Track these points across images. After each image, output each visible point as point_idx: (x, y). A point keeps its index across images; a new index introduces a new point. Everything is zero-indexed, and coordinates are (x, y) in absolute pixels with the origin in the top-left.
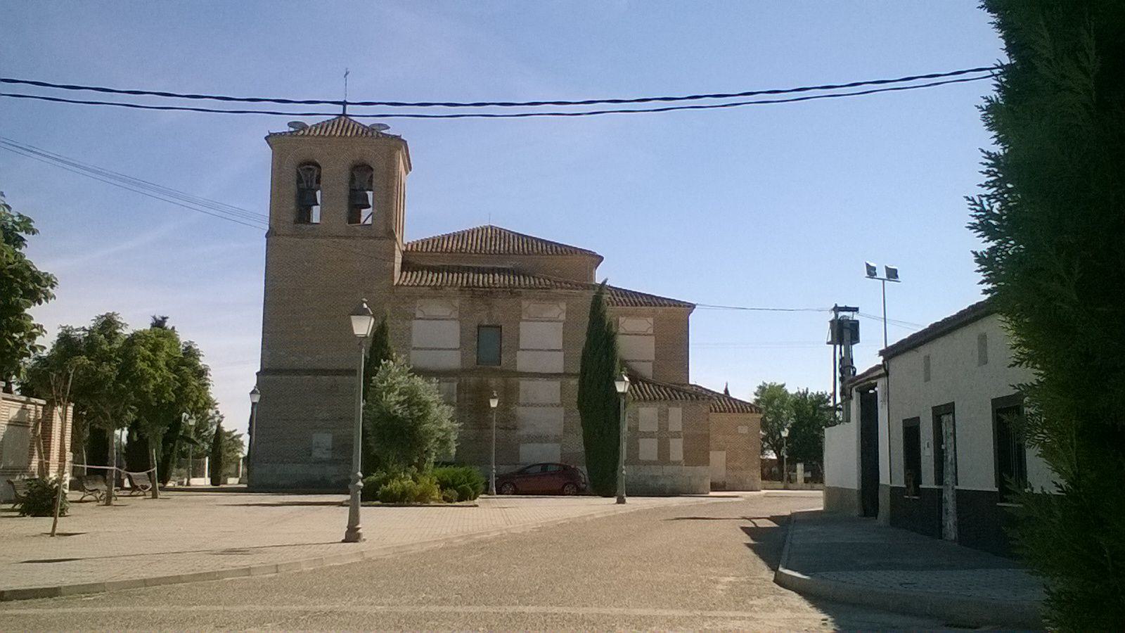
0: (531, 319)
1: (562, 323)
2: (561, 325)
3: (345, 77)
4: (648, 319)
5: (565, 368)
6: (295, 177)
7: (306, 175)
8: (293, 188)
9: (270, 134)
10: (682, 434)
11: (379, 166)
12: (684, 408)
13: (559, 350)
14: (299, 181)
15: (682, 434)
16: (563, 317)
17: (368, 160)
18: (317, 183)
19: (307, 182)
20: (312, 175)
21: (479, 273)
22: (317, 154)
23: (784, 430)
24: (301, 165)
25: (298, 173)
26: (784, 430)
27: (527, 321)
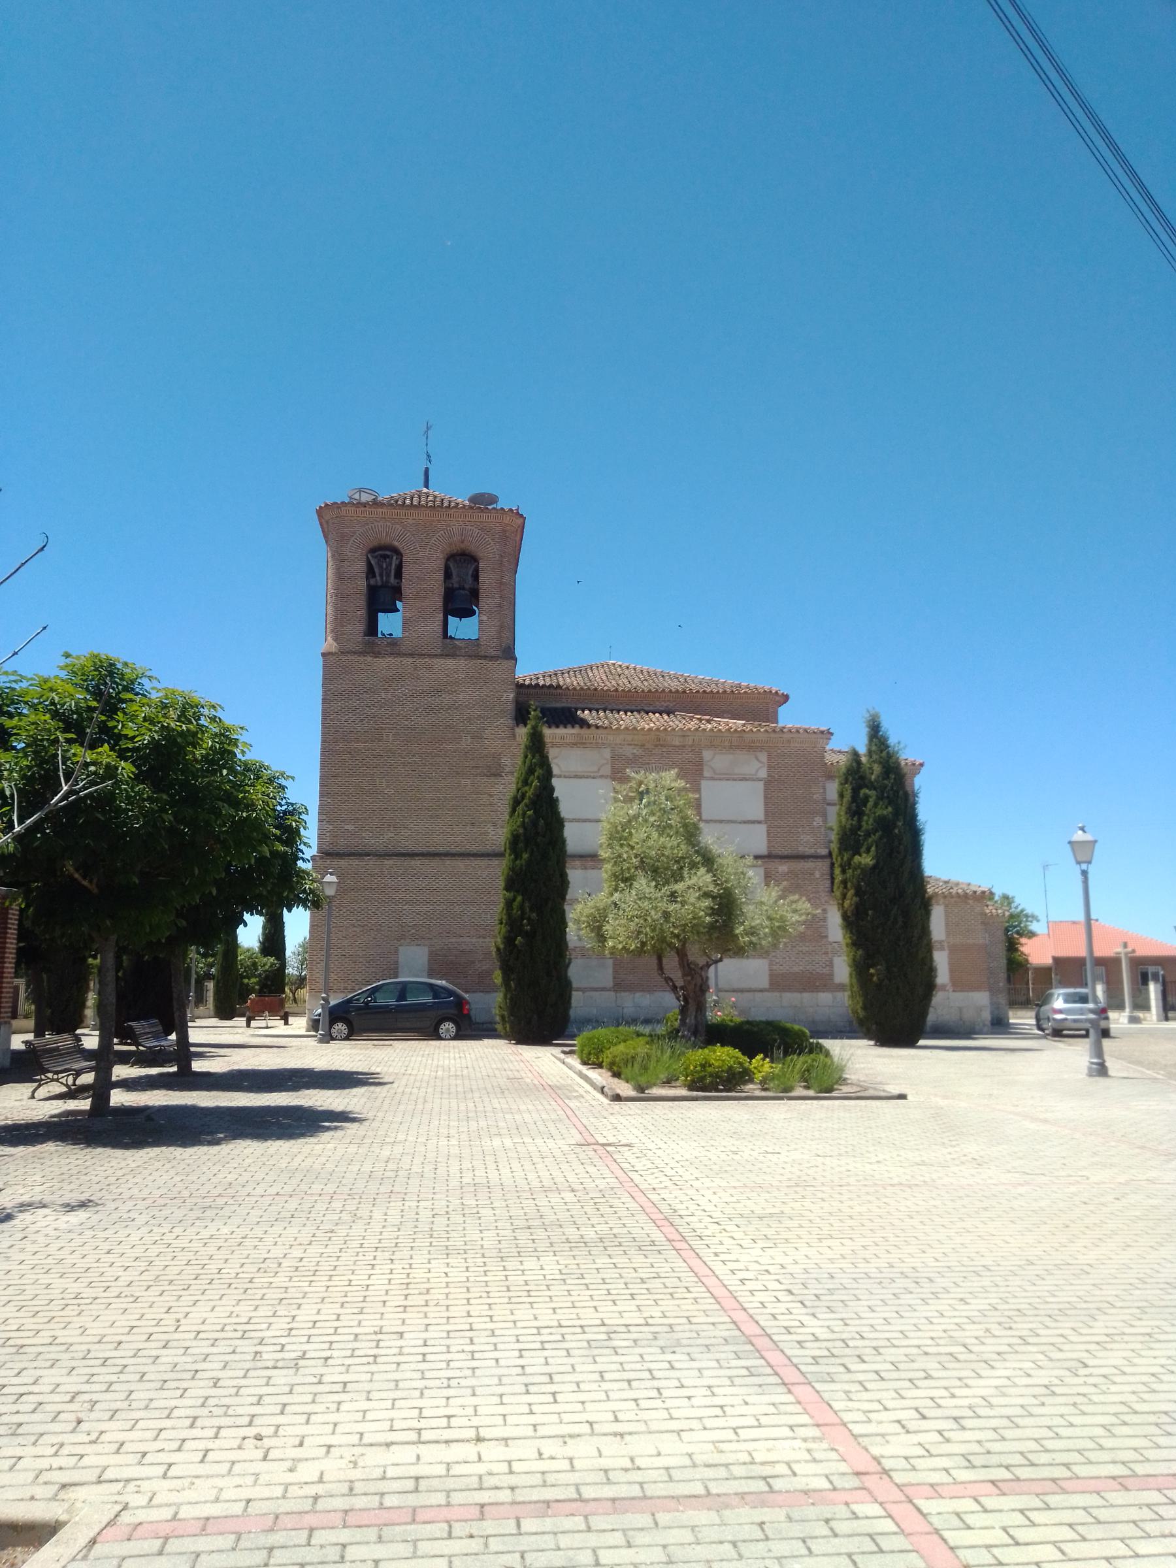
0: (716, 776)
1: (762, 783)
2: (761, 785)
3: (920, 1444)
4: (758, 754)
5: (768, 847)
6: (364, 568)
7: (381, 567)
8: (361, 585)
9: (327, 505)
10: (946, 944)
11: (488, 552)
12: (946, 906)
13: (759, 822)
14: (370, 572)
15: (946, 944)
16: (763, 773)
17: (472, 547)
18: (396, 577)
19: (381, 575)
20: (390, 564)
21: (7, 933)
22: (392, 533)
23: (679, 776)
24: (373, 551)
25: (368, 558)
26: (679, 776)
27: (712, 779)
